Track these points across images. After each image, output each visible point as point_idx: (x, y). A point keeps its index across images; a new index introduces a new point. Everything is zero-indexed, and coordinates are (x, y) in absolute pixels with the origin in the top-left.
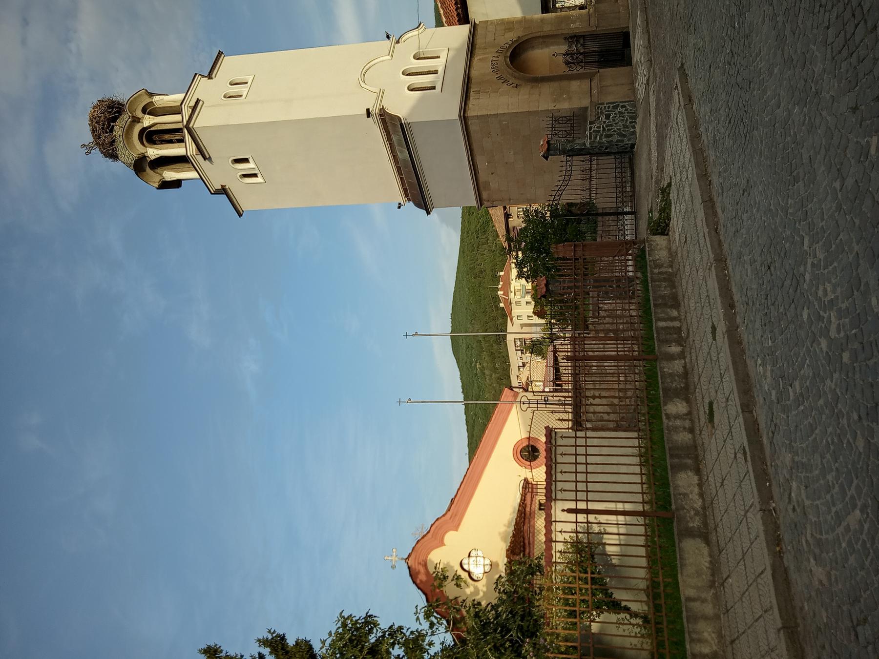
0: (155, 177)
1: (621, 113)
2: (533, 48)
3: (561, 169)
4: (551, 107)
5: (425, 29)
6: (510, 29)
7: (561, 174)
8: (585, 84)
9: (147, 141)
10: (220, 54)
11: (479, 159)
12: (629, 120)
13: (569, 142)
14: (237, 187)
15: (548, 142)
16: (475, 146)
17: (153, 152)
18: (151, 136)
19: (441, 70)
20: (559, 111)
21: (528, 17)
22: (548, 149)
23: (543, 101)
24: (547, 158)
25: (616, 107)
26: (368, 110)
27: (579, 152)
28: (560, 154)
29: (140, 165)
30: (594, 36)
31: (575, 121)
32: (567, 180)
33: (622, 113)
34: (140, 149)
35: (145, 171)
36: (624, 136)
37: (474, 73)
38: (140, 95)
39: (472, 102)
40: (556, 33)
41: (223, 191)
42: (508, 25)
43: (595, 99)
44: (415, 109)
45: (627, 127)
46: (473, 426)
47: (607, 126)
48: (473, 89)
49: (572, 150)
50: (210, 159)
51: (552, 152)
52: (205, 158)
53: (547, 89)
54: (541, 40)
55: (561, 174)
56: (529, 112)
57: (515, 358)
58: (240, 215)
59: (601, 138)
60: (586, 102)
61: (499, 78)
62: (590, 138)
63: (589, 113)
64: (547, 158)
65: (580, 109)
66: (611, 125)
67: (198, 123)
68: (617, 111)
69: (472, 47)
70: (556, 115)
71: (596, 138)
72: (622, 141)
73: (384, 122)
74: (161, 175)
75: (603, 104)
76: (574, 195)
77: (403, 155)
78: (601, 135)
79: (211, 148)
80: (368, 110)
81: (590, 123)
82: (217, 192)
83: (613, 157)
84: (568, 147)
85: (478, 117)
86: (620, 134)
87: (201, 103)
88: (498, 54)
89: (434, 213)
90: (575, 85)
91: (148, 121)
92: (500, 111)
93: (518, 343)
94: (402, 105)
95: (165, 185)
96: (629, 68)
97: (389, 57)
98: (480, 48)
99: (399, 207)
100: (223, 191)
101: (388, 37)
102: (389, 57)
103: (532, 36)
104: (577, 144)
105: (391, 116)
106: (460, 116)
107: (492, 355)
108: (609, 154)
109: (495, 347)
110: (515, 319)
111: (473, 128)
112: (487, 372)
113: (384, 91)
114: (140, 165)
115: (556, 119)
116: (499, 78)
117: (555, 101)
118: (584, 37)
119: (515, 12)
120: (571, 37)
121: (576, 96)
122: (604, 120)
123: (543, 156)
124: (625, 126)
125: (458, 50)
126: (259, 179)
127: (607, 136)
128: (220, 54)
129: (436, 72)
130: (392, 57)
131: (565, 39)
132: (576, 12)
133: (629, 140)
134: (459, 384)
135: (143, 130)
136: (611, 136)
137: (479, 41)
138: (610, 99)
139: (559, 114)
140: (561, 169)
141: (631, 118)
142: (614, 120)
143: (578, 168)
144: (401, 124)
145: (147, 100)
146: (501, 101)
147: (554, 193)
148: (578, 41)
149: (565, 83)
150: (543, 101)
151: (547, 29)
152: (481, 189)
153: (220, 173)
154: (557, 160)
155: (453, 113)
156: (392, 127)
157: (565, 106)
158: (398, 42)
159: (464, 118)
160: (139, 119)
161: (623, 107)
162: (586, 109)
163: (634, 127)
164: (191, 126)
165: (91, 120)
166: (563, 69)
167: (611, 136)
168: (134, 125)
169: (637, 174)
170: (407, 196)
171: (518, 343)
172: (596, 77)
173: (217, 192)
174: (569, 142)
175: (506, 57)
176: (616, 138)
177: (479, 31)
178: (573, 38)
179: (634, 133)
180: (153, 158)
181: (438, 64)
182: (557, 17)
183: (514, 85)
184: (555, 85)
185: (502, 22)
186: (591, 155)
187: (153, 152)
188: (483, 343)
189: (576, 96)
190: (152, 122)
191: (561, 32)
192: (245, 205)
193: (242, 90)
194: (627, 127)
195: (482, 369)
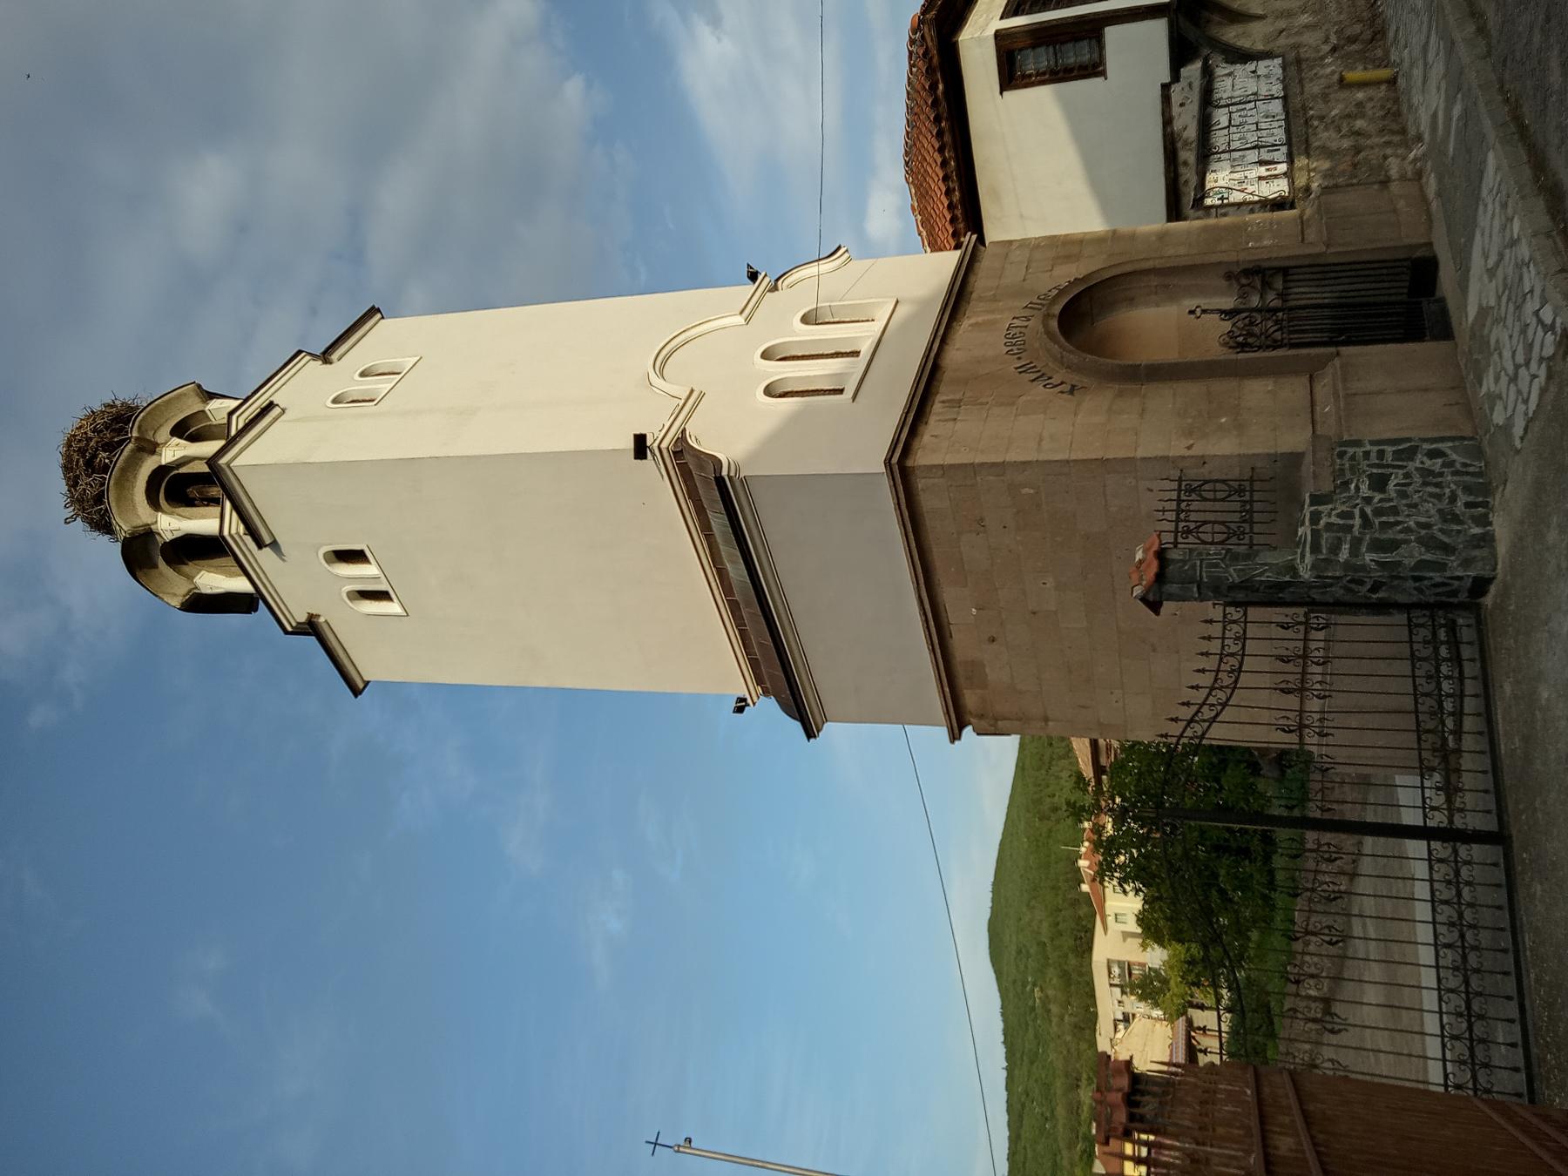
0: (176, 584)
1: (1426, 473)
2: (1131, 301)
3: (1205, 646)
4: (1178, 448)
5: (850, 259)
6: (1068, 258)
7: (1204, 663)
8: (1293, 390)
9: (169, 499)
10: (373, 311)
11: (949, 596)
12: (1463, 498)
13: (1235, 557)
14: (354, 626)
15: (1161, 555)
16: (937, 555)
17: (172, 524)
18: (177, 488)
19: (865, 348)
20: (1203, 461)
21: (1124, 227)
22: (1160, 577)
23: (1152, 431)
24: (1155, 607)
25: (1411, 453)
26: (640, 440)
27: (1273, 595)
28: (1202, 598)
29: (141, 553)
30: (1320, 270)
31: (1261, 492)
32: (1228, 676)
33: (1430, 472)
34: (143, 513)
35: (155, 566)
36: (1448, 549)
37: (955, 356)
38: (178, 397)
39: (935, 426)
40: (1198, 261)
41: (311, 627)
42: (1065, 247)
43: (1328, 428)
44: (774, 440)
45: (1456, 519)
46: (1021, 1117)
47: (1379, 512)
48: (943, 394)
49: (1246, 585)
50: (274, 545)
51: (1173, 588)
52: (260, 544)
53: (1164, 399)
54: (1155, 281)
55: (1204, 663)
56: (1103, 462)
57: (1109, 1001)
58: (356, 692)
59: (1355, 552)
60: (1295, 439)
61: (1023, 370)
62: (1316, 548)
63: (1307, 467)
64: (1155, 607)
65: (1274, 458)
66: (1394, 511)
67: (246, 460)
68: (1411, 466)
69: (958, 298)
70: (1192, 473)
71: (1335, 549)
72: (1441, 567)
73: (686, 474)
74: (190, 578)
75: (1357, 443)
76: (1251, 723)
77: (737, 571)
78: (1356, 544)
79: (276, 516)
80: (640, 440)
81: (1316, 500)
82: (299, 630)
83: (1400, 618)
84: (1233, 575)
85: (945, 469)
86: (1429, 543)
87: (276, 411)
88: (1027, 313)
89: (830, 730)
90: (1257, 391)
91: (173, 451)
92: (1013, 456)
93: (1116, 970)
94: (735, 434)
95: (200, 603)
96: (1443, 346)
97: (740, 320)
98: (980, 299)
99: (740, 710)
100: (311, 627)
101: (753, 276)
102: (740, 320)
103: (1128, 268)
104: (1268, 564)
105: (698, 454)
106: (888, 462)
107: (1065, 976)
108: (1382, 607)
109: (1073, 961)
110: (1110, 920)
111: (928, 502)
112: (1054, 1009)
113: (702, 395)
114: (141, 553)
115: (1191, 487)
116: (1023, 370)
117: (1189, 433)
118: (1285, 271)
119: (1086, 219)
120: (1247, 272)
121: (1265, 419)
122: (1365, 490)
123: (1143, 599)
124: (1449, 517)
125: (924, 303)
126: (392, 608)
127: (1377, 546)
128: (373, 311)
129: (856, 354)
130: (748, 320)
131: (1229, 276)
132: (1259, 217)
133: (1467, 563)
134: (999, 1025)
135: (161, 471)
136: (1393, 545)
137: (981, 282)
138: (1384, 429)
139: (1204, 472)
140: (1205, 646)
141: (1468, 489)
142: (1403, 495)
143: (1265, 648)
144: (720, 481)
145: (194, 406)
146: (1020, 429)
147: (1186, 713)
148: (1266, 285)
149: (1221, 386)
150: (1152, 431)
151: (1177, 253)
152: (961, 680)
153: (300, 583)
154: (1192, 622)
155: (871, 455)
156: (714, 495)
157: (1223, 447)
158: (775, 288)
159: (901, 467)
160: (156, 445)
161: (1433, 454)
162: (1295, 459)
163: (1484, 521)
164: (223, 461)
165: (69, 445)
166: (1217, 352)
167: (1393, 545)
168: (142, 460)
169: (1506, 688)
170: (759, 680)
171: (1116, 970)
172: (1329, 370)
173: (299, 630)
174: (1235, 557)
175: (1047, 316)
176: (1411, 554)
177: (986, 263)
178: (1254, 275)
179: (1487, 540)
180: (168, 537)
181: (864, 336)
182: (1205, 229)
183: (1066, 387)
184: (1194, 389)
185: (1053, 241)
186: (1313, 605)
187: (172, 524)
188: (1049, 948)
189: (1265, 419)
190: (179, 454)
191: (1214, 258)
192: (370, 664)
193: (381, 385)
194: (1456, 519)
195: (1046, 1001)
